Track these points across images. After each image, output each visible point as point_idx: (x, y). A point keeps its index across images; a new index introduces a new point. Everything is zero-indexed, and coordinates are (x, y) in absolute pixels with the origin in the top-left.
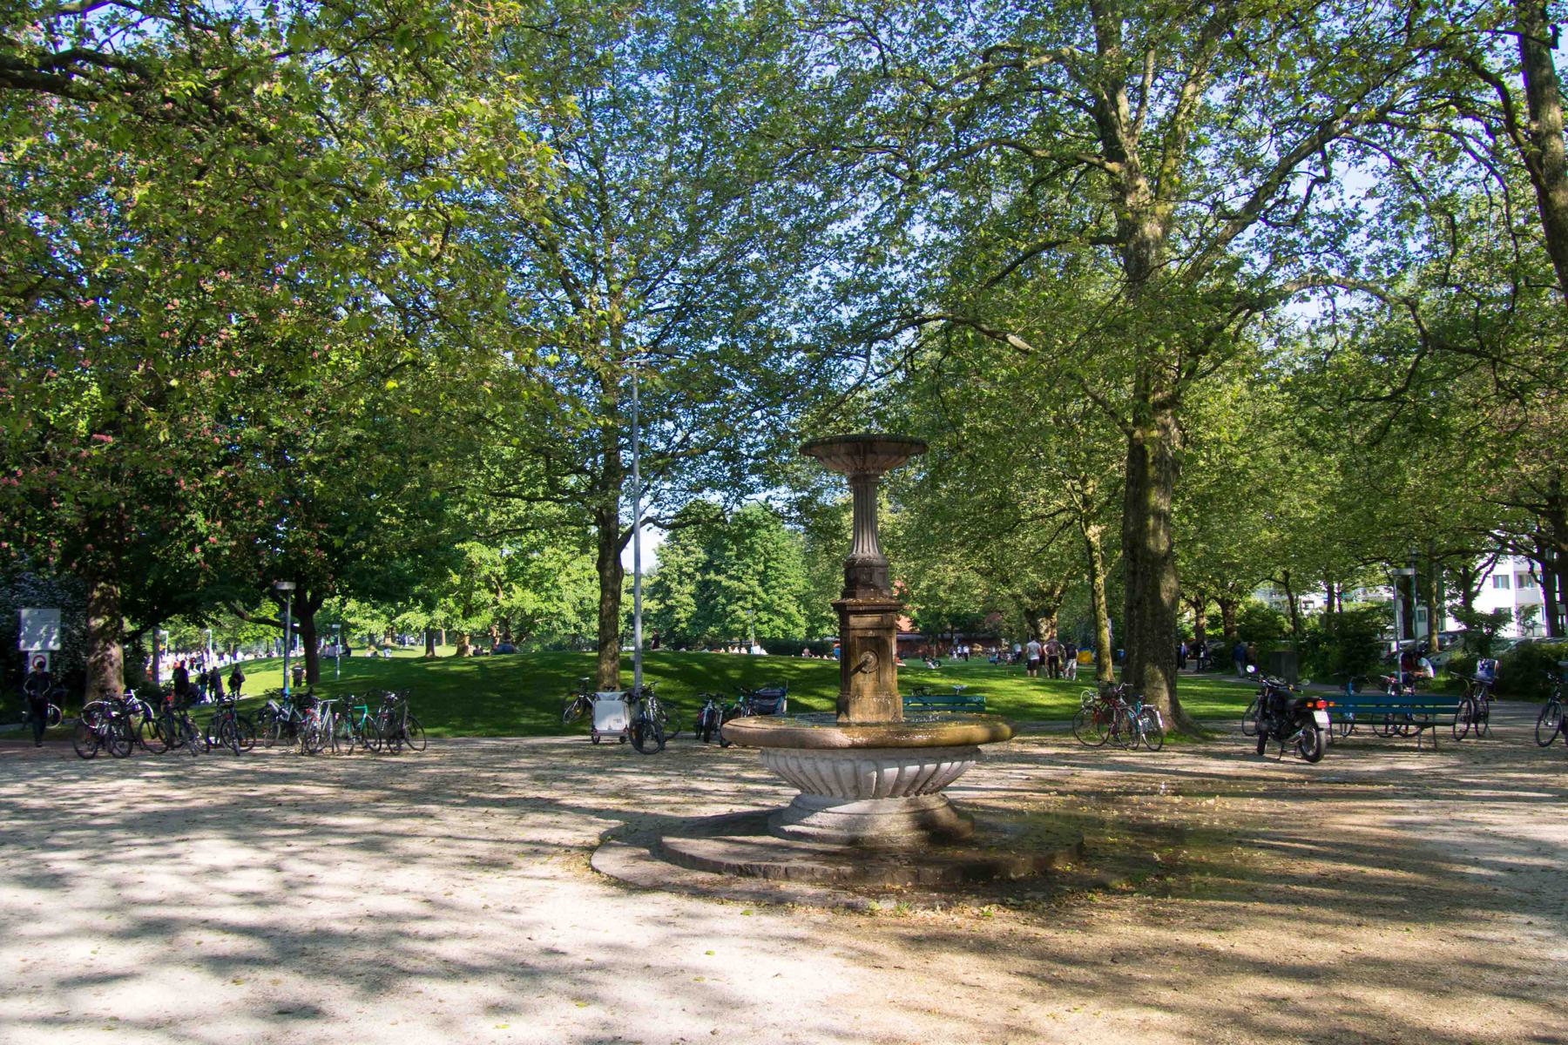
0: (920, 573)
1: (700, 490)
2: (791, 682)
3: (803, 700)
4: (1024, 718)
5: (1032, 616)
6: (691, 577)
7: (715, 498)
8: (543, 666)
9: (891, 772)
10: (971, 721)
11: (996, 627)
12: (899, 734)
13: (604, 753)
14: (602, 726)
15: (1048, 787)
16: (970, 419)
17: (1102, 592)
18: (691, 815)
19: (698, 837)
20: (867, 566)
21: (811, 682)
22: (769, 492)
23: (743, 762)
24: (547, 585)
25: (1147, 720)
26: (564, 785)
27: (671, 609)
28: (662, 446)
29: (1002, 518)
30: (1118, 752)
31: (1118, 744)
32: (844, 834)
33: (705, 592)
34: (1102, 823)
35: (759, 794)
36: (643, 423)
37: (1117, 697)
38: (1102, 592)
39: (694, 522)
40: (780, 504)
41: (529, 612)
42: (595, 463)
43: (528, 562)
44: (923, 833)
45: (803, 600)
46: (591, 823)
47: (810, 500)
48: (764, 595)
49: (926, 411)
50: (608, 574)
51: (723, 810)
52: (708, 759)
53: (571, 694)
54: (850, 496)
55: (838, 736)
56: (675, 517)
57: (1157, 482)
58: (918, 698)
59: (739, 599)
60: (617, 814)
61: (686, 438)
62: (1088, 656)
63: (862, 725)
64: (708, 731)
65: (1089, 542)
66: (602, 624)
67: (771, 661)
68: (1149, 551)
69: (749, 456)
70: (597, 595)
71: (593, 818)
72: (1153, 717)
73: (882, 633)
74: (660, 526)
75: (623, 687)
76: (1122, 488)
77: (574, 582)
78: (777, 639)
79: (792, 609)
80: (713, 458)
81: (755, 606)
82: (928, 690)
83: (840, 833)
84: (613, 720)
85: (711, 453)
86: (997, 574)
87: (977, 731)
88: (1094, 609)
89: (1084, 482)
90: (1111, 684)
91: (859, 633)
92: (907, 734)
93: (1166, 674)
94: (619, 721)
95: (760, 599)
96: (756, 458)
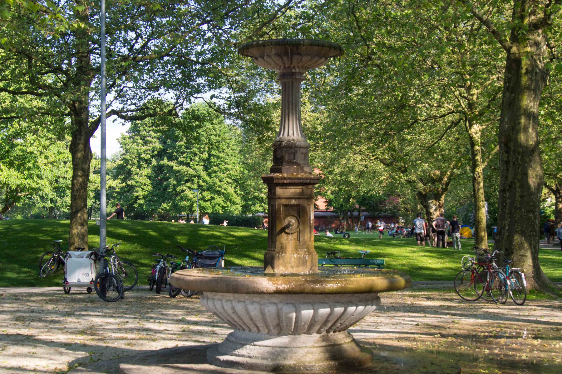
0: (333, 162)
1: (157, 89)
2: (228, 246)
3: (237, 261)
4: (417, 279)
5: (423, 198)
6: (148, 162)
7: (168, 96)
8: (25, 230)
9: (307, 313)
10: (373, 274)
11: (395, 207)
12: (315, 282)
13: (74, 300)
14: (72, 279)
15: (433, 331)
16: (379, 35)
17: (481, 180)
18: (144, 348)
19: (149, 364)
20: (292, 147)
21: (243, 248)
22: (212, 92)
23: (188, 308)
24: (30, 165)
25: (514, 280)
26: (40, 324)
27: (131, 188)
28: (125, 51)
29: (402, 115)
30: (490, 305)
31: (491, 299)
32: (269, 363)
33: (160, 175)
34: (476, 359)
35: (200, 333)
36: (109, 32)
37: (491, 261)
38: (481, 180)
39: (151, 116)
40: (222, 102)
41: (14, 187)
42: (69, 64)
43: (13, 146)
44: (332, 363)
45: (239, 182)
46: (61, 354)
47: (246, 99)
48: (207, 178)
49: (342, 28)
50: (79, 155)
51: (171, 344)
52: (159, 306)
53: (47, 253)
54: (279, 97)
55: (265, 284)
56: (137, 110)
57: (528, 88)
58: (331, 261)
59: (187, 181)
60: (83, 347)
61: (144, 46)
62: (467, 232)
63: (282, 275)
64: (159, 284)
65: (471, 138)
66: (74, 198)
67: (212, 229)
68: (521, 146)
69: (197, 63)
70: (70, 174)
71: (63, 350)
72: (519, 277)
73: (301, 202)
74: (122, 117)
75: (90, 248)
76: (500, 95)
77: (53, 160)
78: (218, 213)
79: (231, 190)
80: (167, 63)
81: (200, 186)
82: (338, 255)
83: (265, 362)
84: (81, 273)
85: (166, 58)
86: (397, 163)
87: (379, 282)
88: (475, 196)
89: (469, 89)
90: (485, 251)
91: (284, 202)
92: (320, 282)
93: (530, 245)
94: (86, 275)
95: (204, 181)
96: (203, 64)
